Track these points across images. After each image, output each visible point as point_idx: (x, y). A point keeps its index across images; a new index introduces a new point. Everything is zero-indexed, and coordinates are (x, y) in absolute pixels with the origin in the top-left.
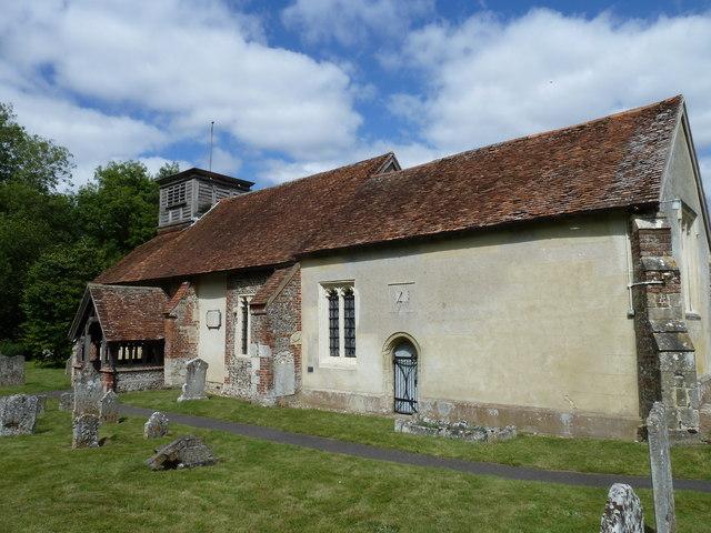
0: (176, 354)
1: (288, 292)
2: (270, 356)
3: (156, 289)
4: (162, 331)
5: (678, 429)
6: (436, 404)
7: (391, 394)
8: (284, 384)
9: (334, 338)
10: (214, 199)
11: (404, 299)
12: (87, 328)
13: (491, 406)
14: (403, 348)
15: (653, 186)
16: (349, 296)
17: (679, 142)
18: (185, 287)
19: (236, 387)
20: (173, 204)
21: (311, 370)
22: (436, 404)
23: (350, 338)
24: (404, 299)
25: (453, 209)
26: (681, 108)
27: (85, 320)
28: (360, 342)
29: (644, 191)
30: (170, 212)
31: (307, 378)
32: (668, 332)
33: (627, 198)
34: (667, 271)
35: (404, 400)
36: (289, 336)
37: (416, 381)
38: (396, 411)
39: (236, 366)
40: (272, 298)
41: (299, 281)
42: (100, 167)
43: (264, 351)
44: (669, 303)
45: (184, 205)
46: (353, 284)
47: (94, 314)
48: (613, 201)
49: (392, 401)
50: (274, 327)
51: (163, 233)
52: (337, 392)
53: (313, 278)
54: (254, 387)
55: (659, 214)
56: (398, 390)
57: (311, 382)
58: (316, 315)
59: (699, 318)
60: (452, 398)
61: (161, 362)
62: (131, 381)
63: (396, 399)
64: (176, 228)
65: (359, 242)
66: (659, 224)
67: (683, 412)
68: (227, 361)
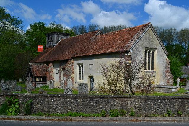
0: (49, 79)
4: (46, 74)
10: (60, 39)
14: (91, 78)
16: (82, 67)
18: (51, 64)
25: (100, 49)
27: (29, 72)
40: (66, 67)
41: (73, 63)
42: (31, 24)
43: (65, 79)
45: (52, 41)
47: (31, 71)
50: (67, 74)
53: (76, 63)
54: (63, 86)
58: (77, 70)
59: (156, 72)
61: (46, 81)
62: (39, 86)
66: (129, 55)
68: (60, 81)
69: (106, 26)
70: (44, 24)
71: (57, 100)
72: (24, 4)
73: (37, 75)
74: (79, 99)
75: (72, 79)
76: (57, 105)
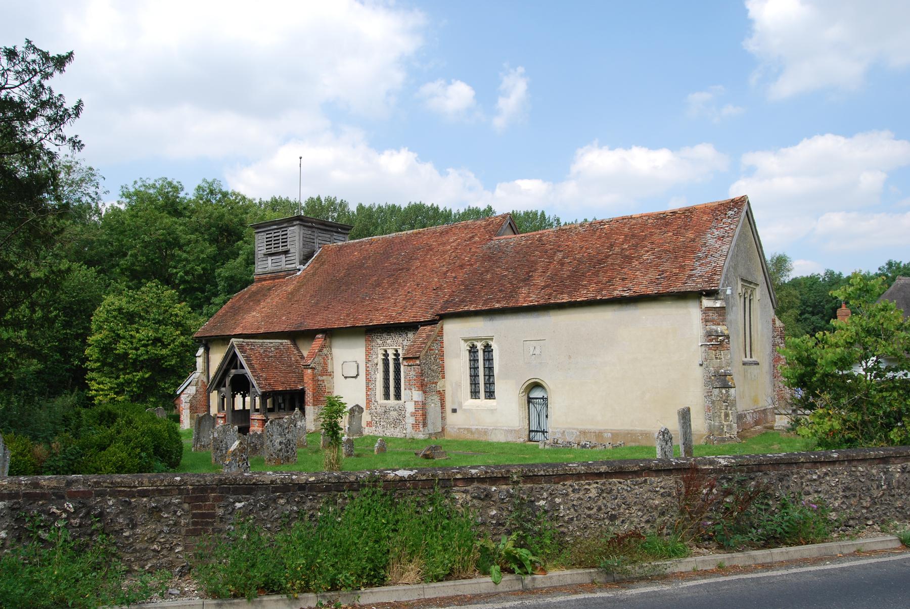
1: (435, 346)
2: (424, 400)
3: (285, 341)
5: (724, 436)
6: (564, 432)
7: (527, 427)
8: (434, 425)
9: (474, 383)
11: (537, 352)
12: (228, 381)
13: (606, 431)
15: (716, 277)
16: (488, 349)
17: (743, 226)
19: (380, 429)
20: (273, 251)
21: (454, 411)
22: (564, 432)
23: (490, 383)
24: (537, 352)
26: (745, 208)
28: (498, 388)
29: (710, 280)
30: (270, 259)
31: (451, 418)
32: (720, 376)
33: (700, 286)
34: (722, 336)
35: (537, 431)
36: (436, 383)
37: (547, 416)
38: (530, 440)
39: (379, 410)
44: (722, 357)
45: (286, 252)
46: (492, 339)
48: (690, 286)
49: (527, 433)
51: (260, 280)
52: (480, 427)
55: (719, 297)
56: (532, 423)
57: (455, 422)
60: (576, 427)
63: (530, 431)
64: (276, 276)
65: (497, 306)
67: (727, 426)
69: (367, 205)
70: (176, 189)
71: (826, 474)
72: (522, 178)
73: (270, 384)
74: (894, 464)
75: (441, 395)
76: (827, 492)
